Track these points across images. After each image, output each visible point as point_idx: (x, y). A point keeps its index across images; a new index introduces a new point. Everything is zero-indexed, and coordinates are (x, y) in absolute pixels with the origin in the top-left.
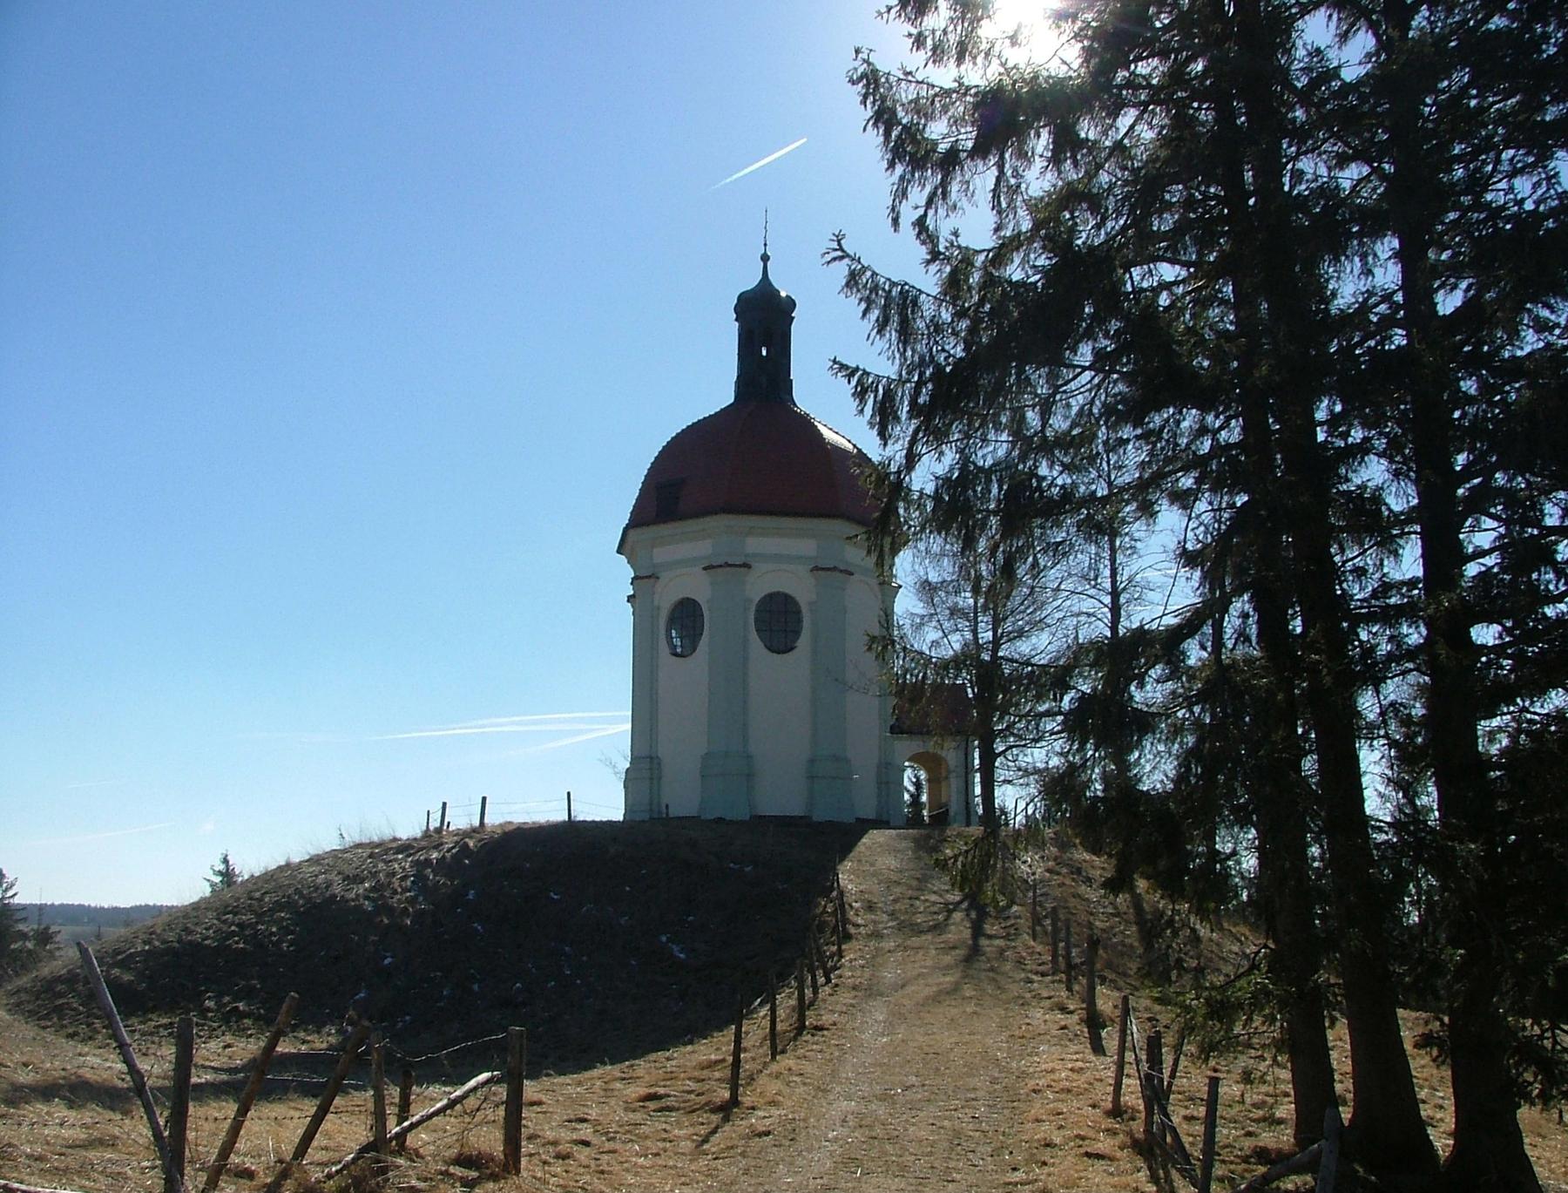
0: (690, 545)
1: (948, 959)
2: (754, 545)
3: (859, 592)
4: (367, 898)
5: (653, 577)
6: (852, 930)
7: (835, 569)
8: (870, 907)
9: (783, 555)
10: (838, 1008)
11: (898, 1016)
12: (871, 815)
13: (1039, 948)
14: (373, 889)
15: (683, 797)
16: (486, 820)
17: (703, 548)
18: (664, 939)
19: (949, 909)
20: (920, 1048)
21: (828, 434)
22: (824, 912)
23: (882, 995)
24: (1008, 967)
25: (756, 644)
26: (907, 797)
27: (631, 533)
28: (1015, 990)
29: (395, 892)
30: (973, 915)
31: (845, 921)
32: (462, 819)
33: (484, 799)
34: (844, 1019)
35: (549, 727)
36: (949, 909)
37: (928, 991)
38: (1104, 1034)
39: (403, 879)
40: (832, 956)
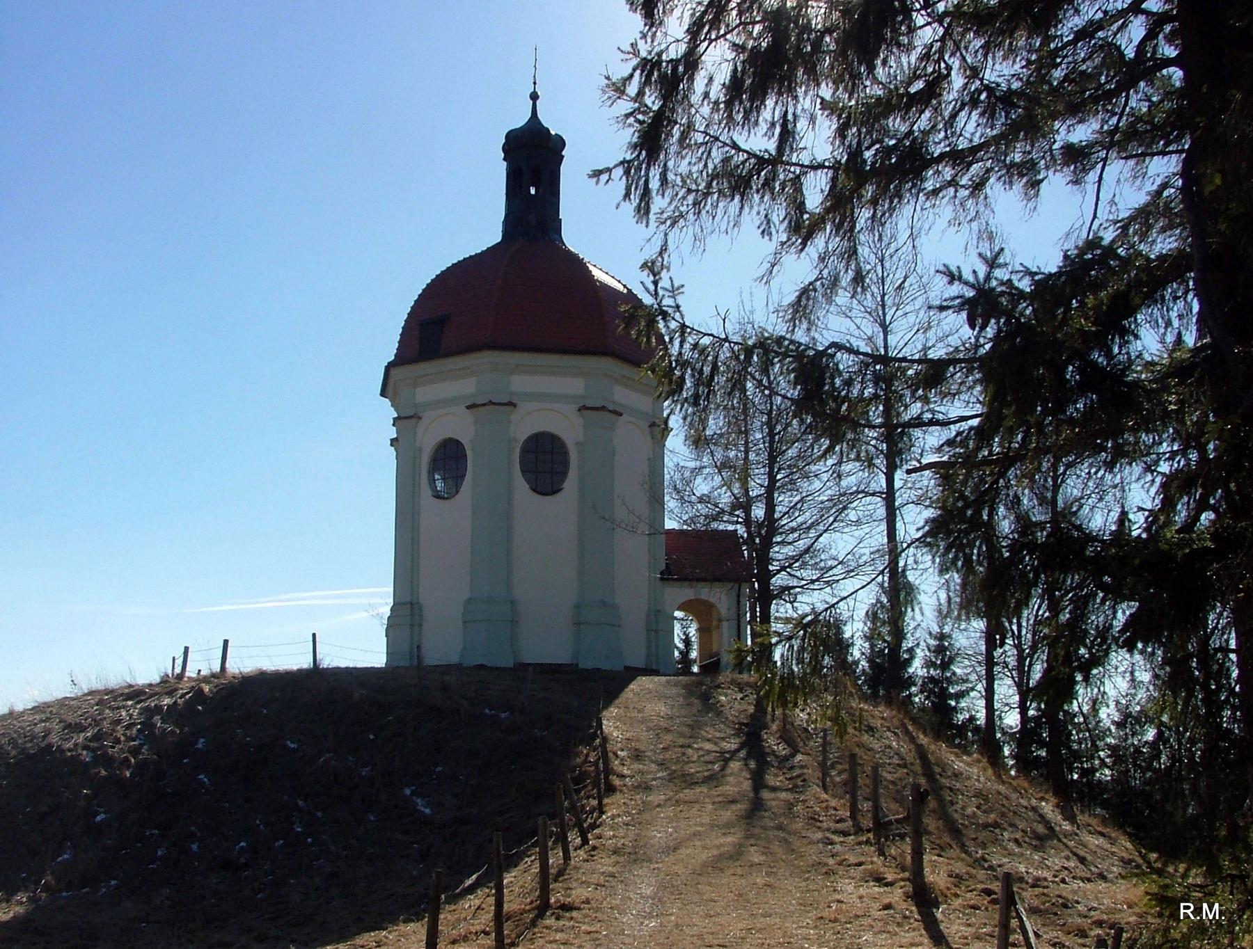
0: (455, 383)
1: (727, 815)
2: (520, 383)
3: (628, 435)
4: (85, 748)
5: (416, 417)
6: (616, 782)
7: (603, 408)
8: (637, 756)
9: (548, 393)
10: (594, 878)
11: (669, 888)
12: (640, 664)
13: (833, 803)
14: (96, 737)
15: (444, 645)
16: (227, 665)
17: (466, 387)
18: (408, 792)
19: (726, 758)
20: (700, 937)
21: (597, 274)
22: (586, 761)
23: (650, 861)
24: (799, 825)
25: (521, 485)
26: (676, 653)
27: (394, 372)
28: (813, 854)
29: (118, 741)
30: (752, 765)
31: (608, 771)
32: (203, 664)
33: (226, 642)
34: (601, 893)
35: (350, 601)
36: (726, 758)
37: (705, 855)
38: (939, 915)
39: (129, 727)
40: (592, 812)
